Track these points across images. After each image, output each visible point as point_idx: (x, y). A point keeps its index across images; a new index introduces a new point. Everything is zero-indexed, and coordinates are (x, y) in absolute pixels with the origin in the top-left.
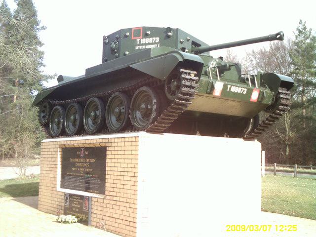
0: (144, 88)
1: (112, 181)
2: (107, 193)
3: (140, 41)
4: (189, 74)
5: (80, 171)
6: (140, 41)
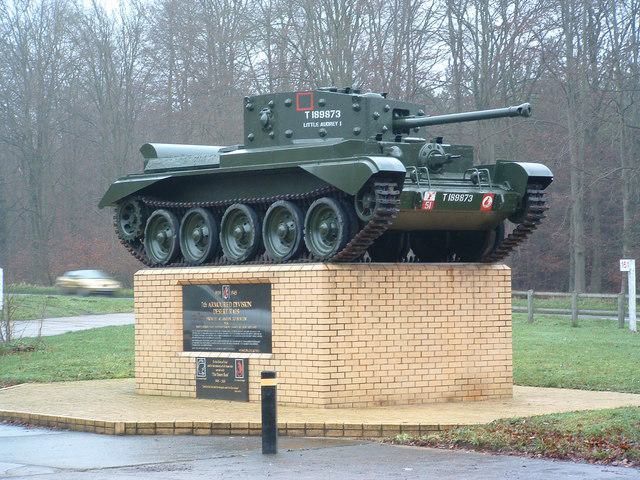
0: (325, 200)
1: (282, 333)
2: (274, 350)
3: (310, 115)
4: (386, 188)
5: (223, 322)
6: (310, 115)
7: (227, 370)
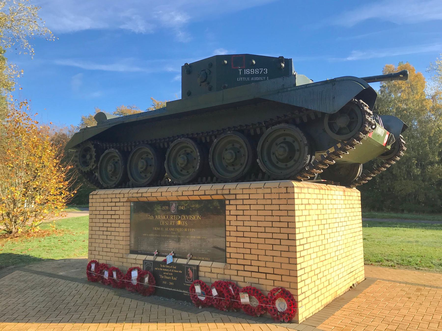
3: (243, 72)
6: (243, 72)
7: (175, 275)
